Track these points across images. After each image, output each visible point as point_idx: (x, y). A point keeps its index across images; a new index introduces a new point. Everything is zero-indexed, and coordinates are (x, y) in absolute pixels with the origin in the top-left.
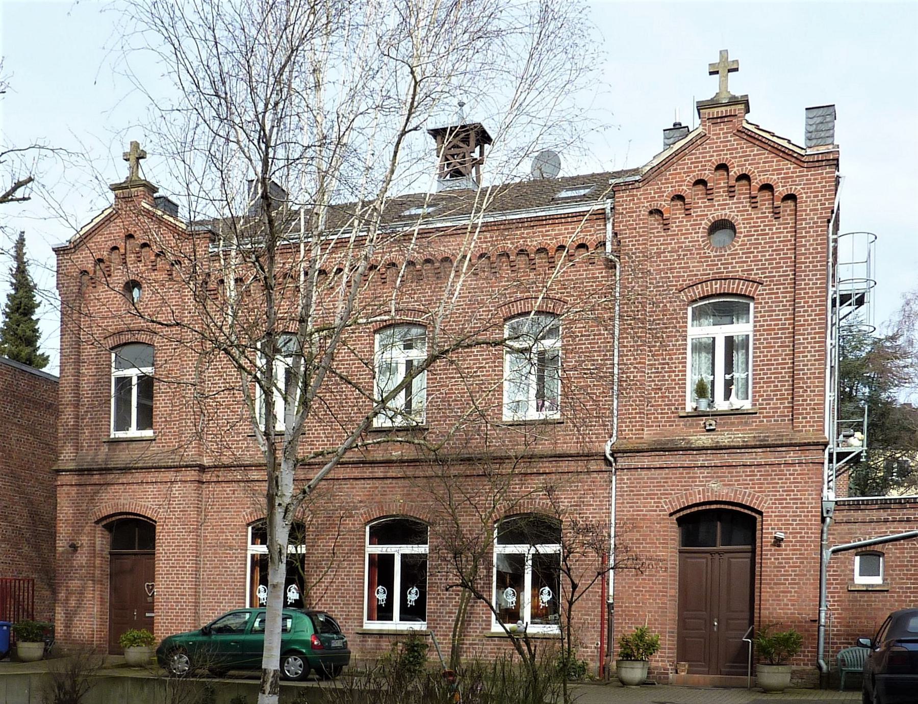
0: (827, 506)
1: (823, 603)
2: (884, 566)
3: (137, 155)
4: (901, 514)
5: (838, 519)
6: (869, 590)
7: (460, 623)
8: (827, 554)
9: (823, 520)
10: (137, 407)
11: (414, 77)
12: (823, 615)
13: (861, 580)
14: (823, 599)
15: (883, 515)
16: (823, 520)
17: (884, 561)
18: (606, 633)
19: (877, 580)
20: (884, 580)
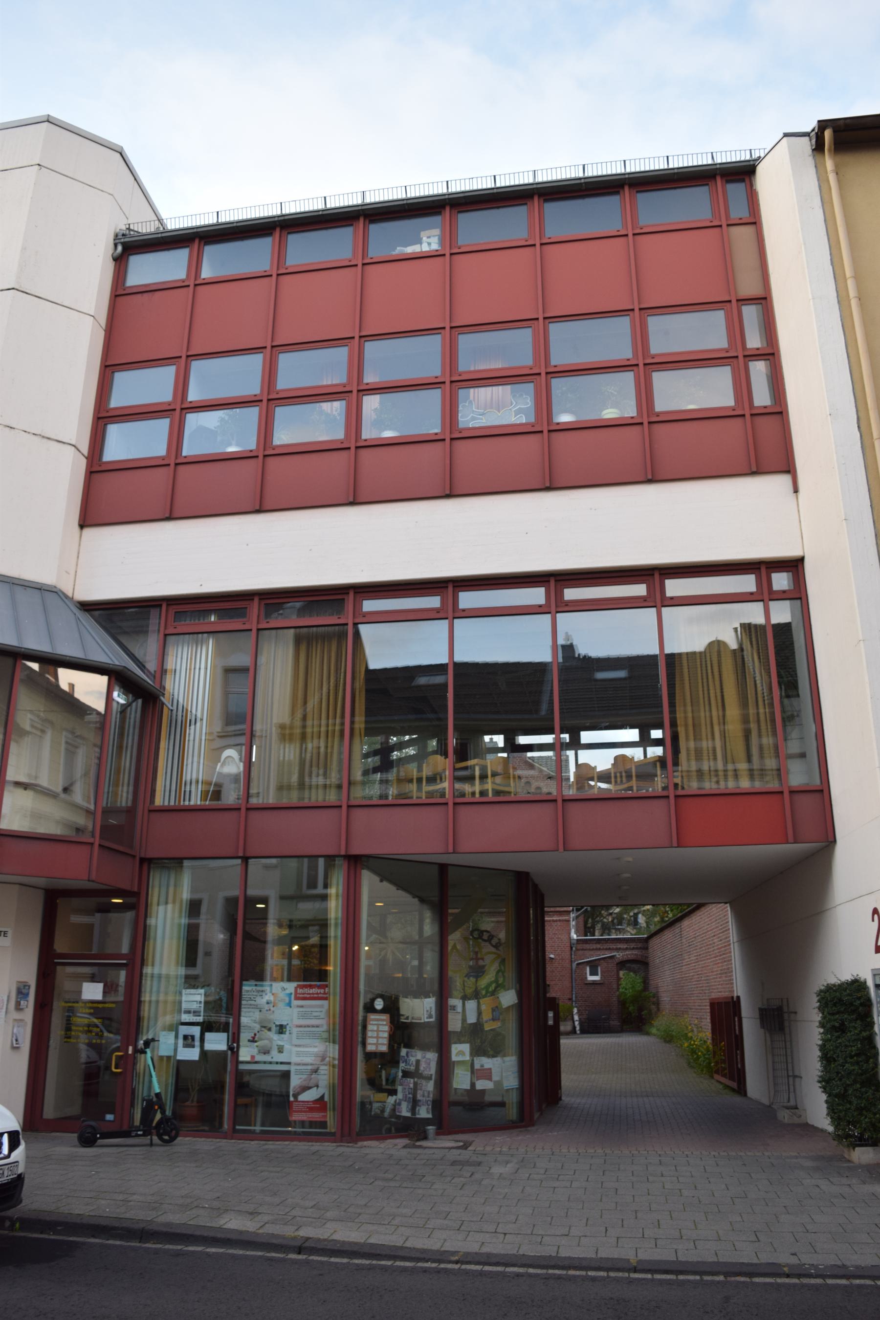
0: (572, 942)
1: (574, 990)
2: (601, 971)
3: (288, 1024)
4: (606, 946)
5: (578, 948)
6: (594, 983)
7: (434, 1265)
8: (574, 965)
9: (571, 948)
10: (837, 1284)
11: (460, 1227)
12: (574, 996)
13: (591, 978)
14: (574, 988)
15: (598, 946)
16: (571, 948)
17: (601, 969)
18: (540, 955)
19: (596, 978)
20: (601, 978)
